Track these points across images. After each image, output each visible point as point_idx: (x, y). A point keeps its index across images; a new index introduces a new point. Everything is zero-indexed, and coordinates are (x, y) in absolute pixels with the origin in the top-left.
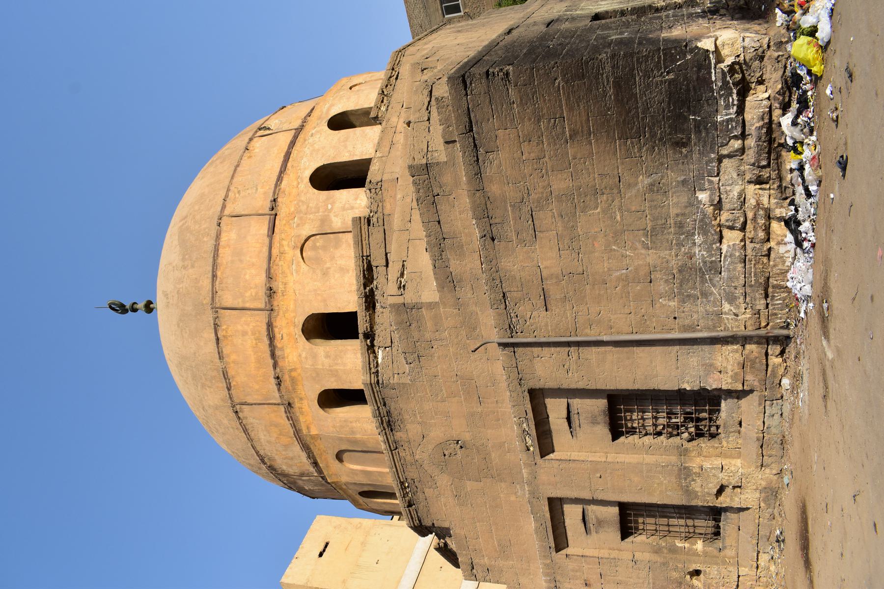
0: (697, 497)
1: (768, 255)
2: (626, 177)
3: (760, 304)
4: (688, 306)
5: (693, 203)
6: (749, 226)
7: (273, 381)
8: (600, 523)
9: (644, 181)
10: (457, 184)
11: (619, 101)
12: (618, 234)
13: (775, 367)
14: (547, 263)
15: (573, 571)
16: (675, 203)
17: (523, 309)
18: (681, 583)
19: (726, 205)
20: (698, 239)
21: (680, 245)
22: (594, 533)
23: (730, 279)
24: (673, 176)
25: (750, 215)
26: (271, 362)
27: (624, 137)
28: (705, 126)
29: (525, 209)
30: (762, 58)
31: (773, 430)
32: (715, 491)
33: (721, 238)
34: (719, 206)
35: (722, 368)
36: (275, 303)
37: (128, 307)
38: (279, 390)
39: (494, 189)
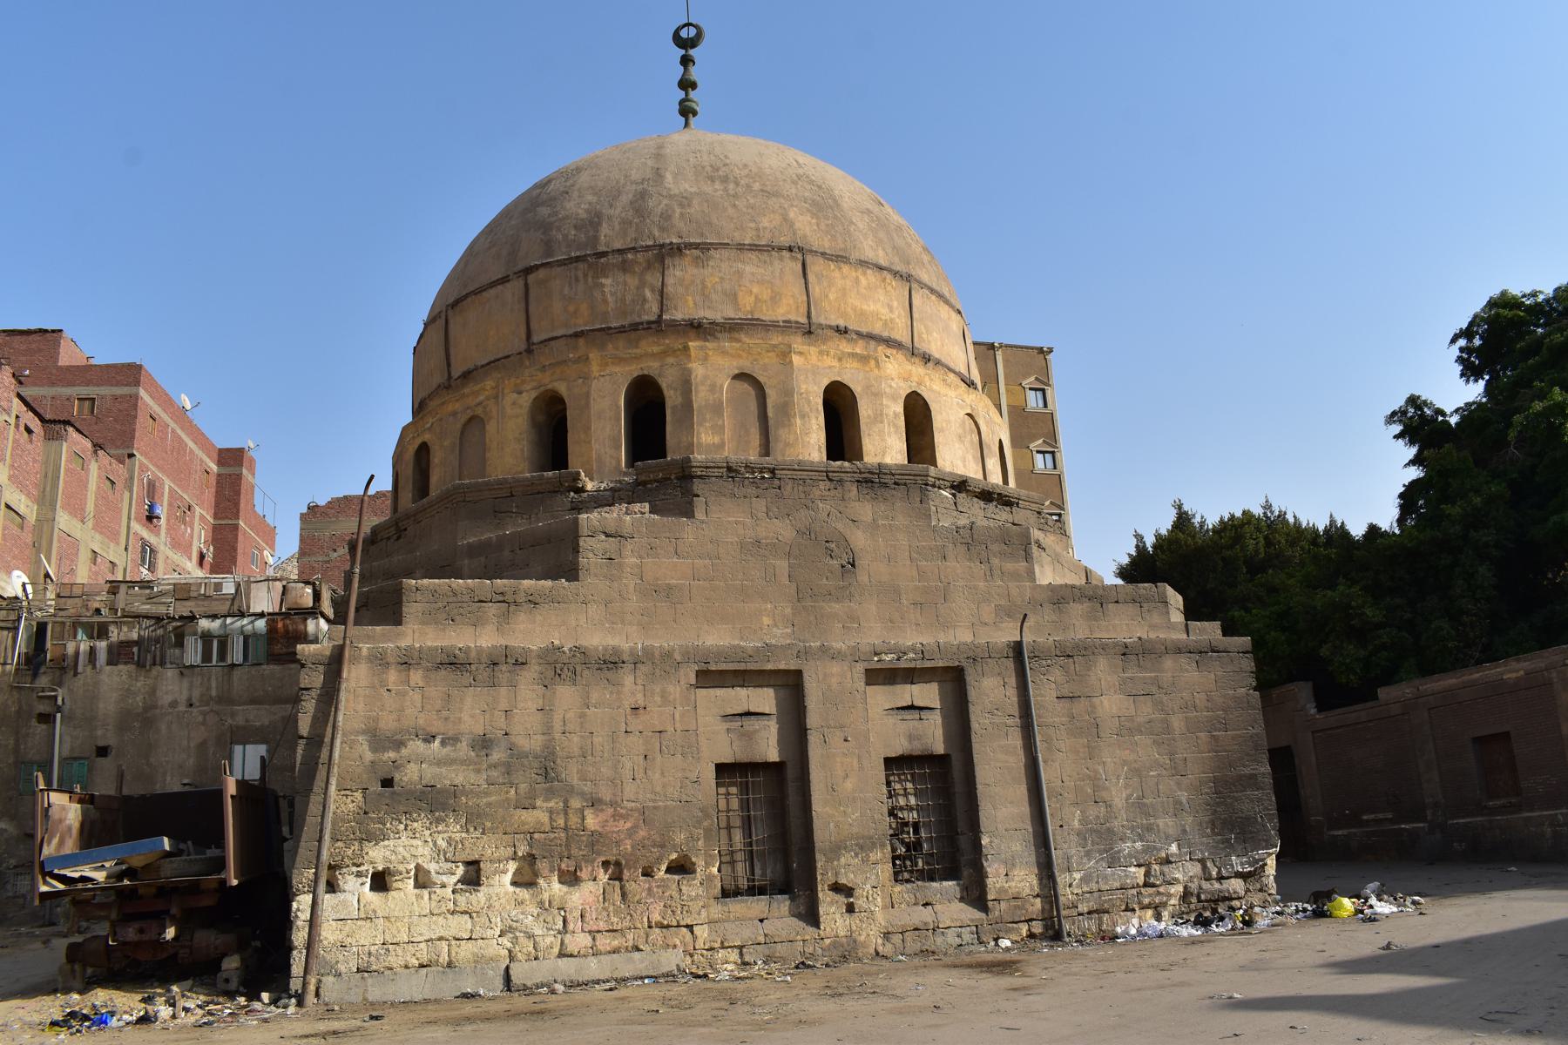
0: (829, 860)
1: (1127, 910)
2: (1185, 781)
3: (1083, 908)
4: (1074, 838)
5: (1168, 839)
6: (1151, 890)
7: (842, 323)
8: (748, 736)
9: (1183, 796)
10: (1153, 627)
11: (1240, 777)
12: (1137, 772)
13: (1018, 930)
14: (1106, 703)
15: (663, 691)
16: (1166, 823)
17: (1057, 674)
18: (662, 846)
19: (1166, 869)
20: (1138, 845)
21: (1133, 829)
22: (725, 726)
23: (1105, 877)
24: (1189, 820)
25: (1161, 889)
26: (864, 330)
27: (1215, 781)
28: (1228, 847)
29: (1154, 689)
30: (1261, 890)
31: (939, 940)
32: (843, 881)
33: (1139, 866)
34: (1167, 861)
35: (1010, 874)
36: (917, 360)
37: (692, 52)
38: (830, 327)
39: (1168, 663)
